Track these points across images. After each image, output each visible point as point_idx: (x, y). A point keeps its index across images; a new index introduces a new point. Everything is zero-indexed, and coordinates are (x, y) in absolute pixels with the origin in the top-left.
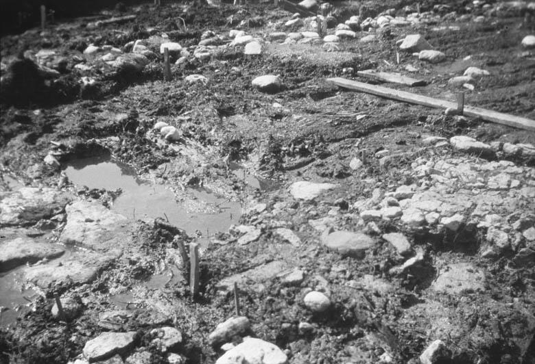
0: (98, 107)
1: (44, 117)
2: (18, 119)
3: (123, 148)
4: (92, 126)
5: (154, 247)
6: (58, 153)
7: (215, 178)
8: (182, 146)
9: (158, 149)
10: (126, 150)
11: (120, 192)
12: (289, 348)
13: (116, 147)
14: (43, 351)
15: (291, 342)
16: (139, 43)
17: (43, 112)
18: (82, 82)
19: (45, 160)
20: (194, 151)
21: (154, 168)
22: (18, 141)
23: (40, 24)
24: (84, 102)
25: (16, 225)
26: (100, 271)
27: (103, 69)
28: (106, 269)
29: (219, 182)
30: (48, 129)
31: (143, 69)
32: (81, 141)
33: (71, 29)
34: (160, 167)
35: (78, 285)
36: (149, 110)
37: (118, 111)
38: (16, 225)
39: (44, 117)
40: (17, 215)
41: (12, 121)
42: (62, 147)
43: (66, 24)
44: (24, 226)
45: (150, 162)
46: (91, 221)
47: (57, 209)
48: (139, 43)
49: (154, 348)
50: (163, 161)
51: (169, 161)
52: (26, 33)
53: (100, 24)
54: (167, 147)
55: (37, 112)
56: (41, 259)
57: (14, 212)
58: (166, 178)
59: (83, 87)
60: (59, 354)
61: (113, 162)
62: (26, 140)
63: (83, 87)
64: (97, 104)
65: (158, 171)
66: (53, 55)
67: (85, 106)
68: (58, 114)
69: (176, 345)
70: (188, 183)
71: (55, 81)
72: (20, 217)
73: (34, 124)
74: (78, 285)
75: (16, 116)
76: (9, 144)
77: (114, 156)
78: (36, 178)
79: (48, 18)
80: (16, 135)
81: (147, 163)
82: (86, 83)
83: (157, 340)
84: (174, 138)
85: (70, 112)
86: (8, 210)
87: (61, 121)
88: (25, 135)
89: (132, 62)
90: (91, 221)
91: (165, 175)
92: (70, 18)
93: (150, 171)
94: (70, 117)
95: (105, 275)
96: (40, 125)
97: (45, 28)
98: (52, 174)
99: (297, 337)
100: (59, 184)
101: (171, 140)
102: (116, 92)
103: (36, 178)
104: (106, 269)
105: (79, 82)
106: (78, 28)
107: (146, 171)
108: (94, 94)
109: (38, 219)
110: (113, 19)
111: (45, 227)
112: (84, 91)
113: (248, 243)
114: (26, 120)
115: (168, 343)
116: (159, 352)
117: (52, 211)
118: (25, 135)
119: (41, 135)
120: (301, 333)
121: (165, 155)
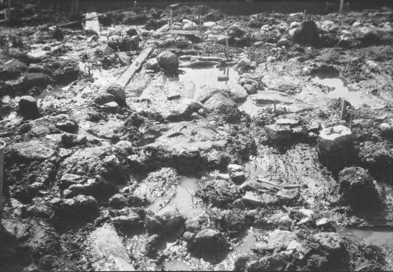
0: (344, 52)
1: (312, 51)
2: (297, 49)
3: (346, 70)
4: (336, 60)
5: (335, 109)
6: (312, 68)
7: (386, 91)
8: (378, 75)
9: (364, 73)
10: (347, 71)
11: (334, 89)
12: (364, 143)
13: (343, 70)
14: (262, 119)
15: (367, 141)
16: (388, 24)
17: (312, 48)
18: (340, 38)
19: (303, 69)
20: (383, 78)
21: (357, 82)
22: (294, 60)
23: (339, 11)
24: (338, 48)
25: (277, 90)
26: (304, 110)
27: (357, 34)
28: (307, 110)
29: (387, 93)
30: (312, 57)
31: (381, 37)
32: (326, 64)
33: (358, 16)
34: (361, 82)
35: (292, 113)
36: (373, 57)
37: (355, 56)
38: (277, 90)
39: (312, 51)
40: (278, 86)
41: (295, 50)
42: (315, 65)
43: (355, 13)
44: (280, 91)
45: (356, 78)
46: (311, 94)
47: (298, 88)
48: (388, 24)
49: (305, 127)
50: (363, 79)
51: (366, 80)
52: (329, 15)
53: (377, 15)
54: (369, 73)
55: (309, 48)
56: (281, 103)
57: (277, 84)
58: (361, 87)
59: (340, 41)
60: (267, 121)
61: (340, 78)
62: (298, 60)
63: (340, 41)
64: (344, 50)
65: (359, 84)
66: (332, 24)
67: (337, 50)
68: (321, 51)
69: (315, 129)
70: (372, 91)
71: (325, 35)
72: (279, 87)
73: (305, 54)
74: (292, 113)
75: (297, 48)
76: (289, 60)
77: (341, 74)
78: (295, 75)
79: (344, 8)
80: (294, 57)
81: (354, 78)
82: (342, 38)
83: (308, 125)
84: (375, 69)
85: (327, 51)
86: (275, 83)
87: (320, 55)
88: (299, 57)
89: (375, 32)
90: (311, 94)
91: (362, 86)
92: (359, 9)
93: (355, 83)
94: (326, 54)
95: (306, 112)
96: (308, 54)
97: (342, 13)
98: (304, 75)
99: (370, 140)
100: (305, 80)
101: (373, 70)
102: (359, 47)
103: (295, 75)
104: (307, 110)
105: (339, 38)
106: (362, 16)
107: (353, 82)
108: (346, 45)
109: (287, 90)
110: (387, 13)
111: (289, 93)
112: (340, 43)
113: (376, 110)
114: (301, 51)
115: (312, 128)
116: (306, 129)
117: (296, 88)
118: (299, 57)
119: (307, 59)
120: (372, 138)
121: (366, 76)
